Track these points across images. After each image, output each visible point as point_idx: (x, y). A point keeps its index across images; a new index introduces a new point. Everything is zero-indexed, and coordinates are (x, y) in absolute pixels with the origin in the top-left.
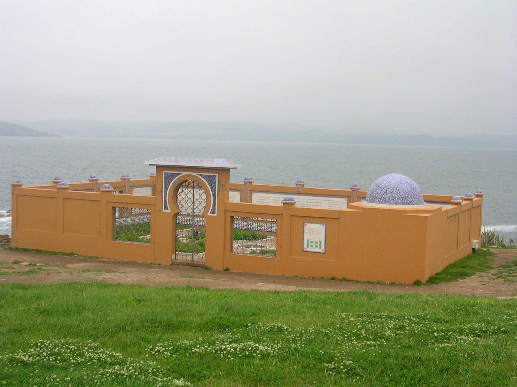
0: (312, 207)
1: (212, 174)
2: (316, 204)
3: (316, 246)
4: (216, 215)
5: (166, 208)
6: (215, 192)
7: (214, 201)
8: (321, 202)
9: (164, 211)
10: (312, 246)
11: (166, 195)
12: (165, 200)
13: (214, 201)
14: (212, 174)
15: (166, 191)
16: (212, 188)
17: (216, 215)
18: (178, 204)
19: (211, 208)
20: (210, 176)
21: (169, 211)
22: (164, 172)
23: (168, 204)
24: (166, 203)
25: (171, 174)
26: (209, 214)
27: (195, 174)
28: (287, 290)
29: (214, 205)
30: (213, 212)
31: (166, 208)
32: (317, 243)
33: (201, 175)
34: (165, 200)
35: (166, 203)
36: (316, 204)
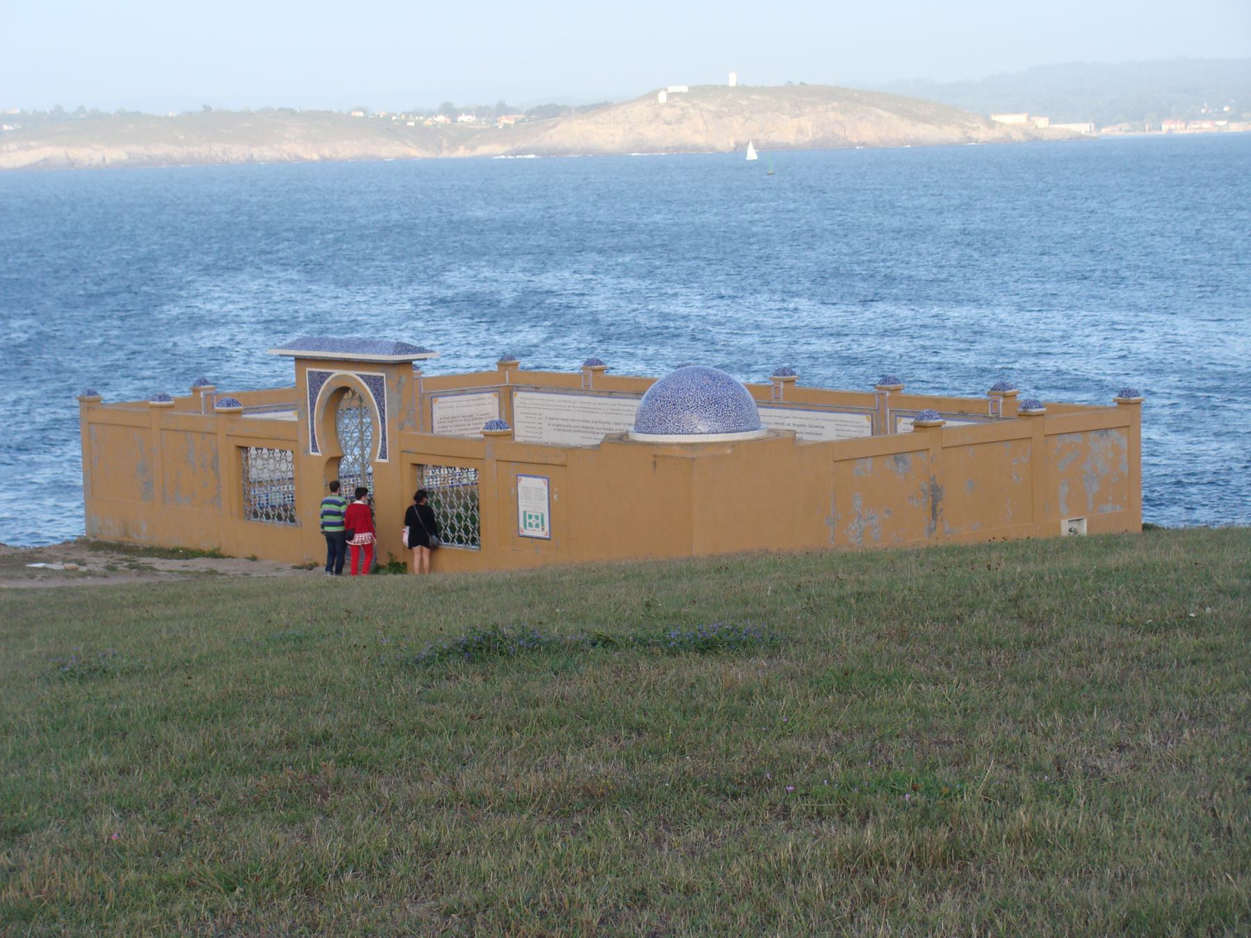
2: (814, 430)
3: (537, 526)
5: (315, 448)
7: (384, 432)
8: (823, 423)
10: (531, 525)
13: (384, 432)
15: (312, 410)
16: (379, 404)
20: (375, 378)
21: (319, 454)
22: (308, 369)
27: (352, 373)
28: (182, 562)
29: (384, 439)
30: (383, 456)
31: (315, 448)
32: (537, 517)
33: (361, 376)
36: (814, 430)
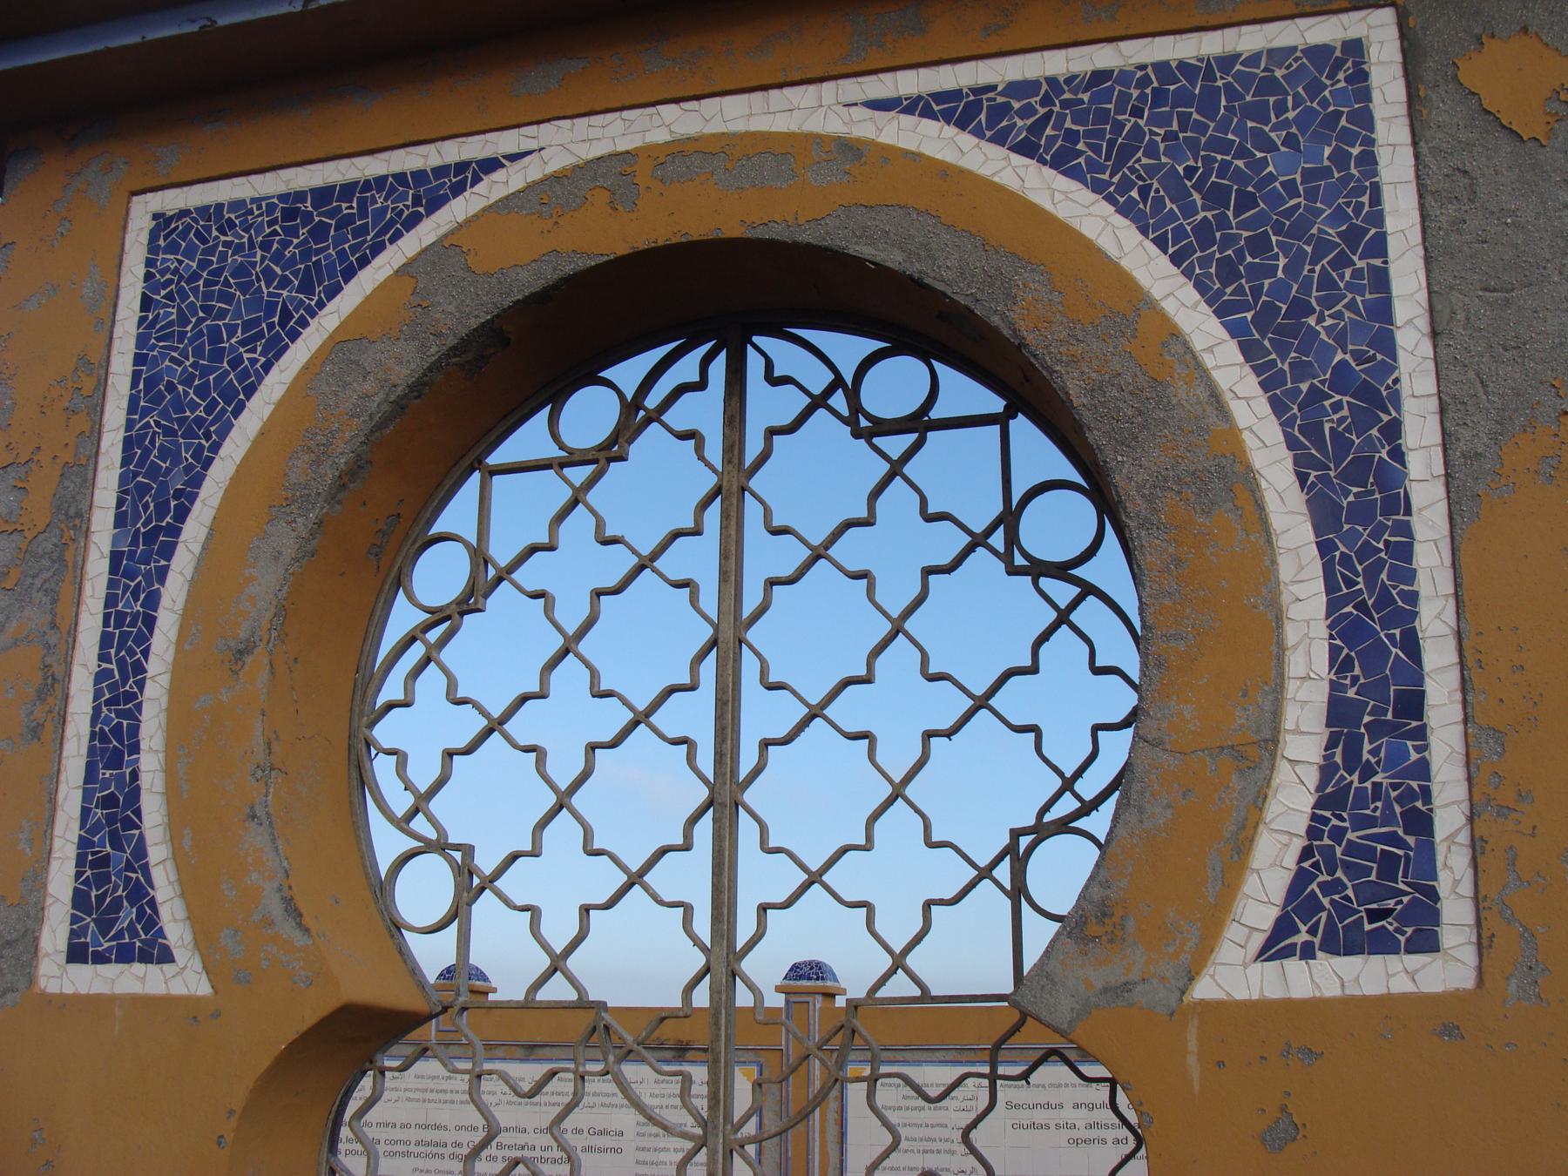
0: (865, 251)
1: (1056, 64)
4: (1448, 969)
5: (115, 916)
6: (1376, 400)
9: (58, 975)
11: (128, 634)
12: (114, 745)
14: (1056, 64)
16: (1268, 333)
17: (1448, 969)
18: (387, 843)
19: (1292, 800)
21: (184, 978)
23: (150, 764)
24: (114, 810)
25: (291, 207)
26: (1235, 974)
30: (1364, 886)
31: (115, 916)
33: (958, 109)
34: (114, 745)
35: (114, 810)
